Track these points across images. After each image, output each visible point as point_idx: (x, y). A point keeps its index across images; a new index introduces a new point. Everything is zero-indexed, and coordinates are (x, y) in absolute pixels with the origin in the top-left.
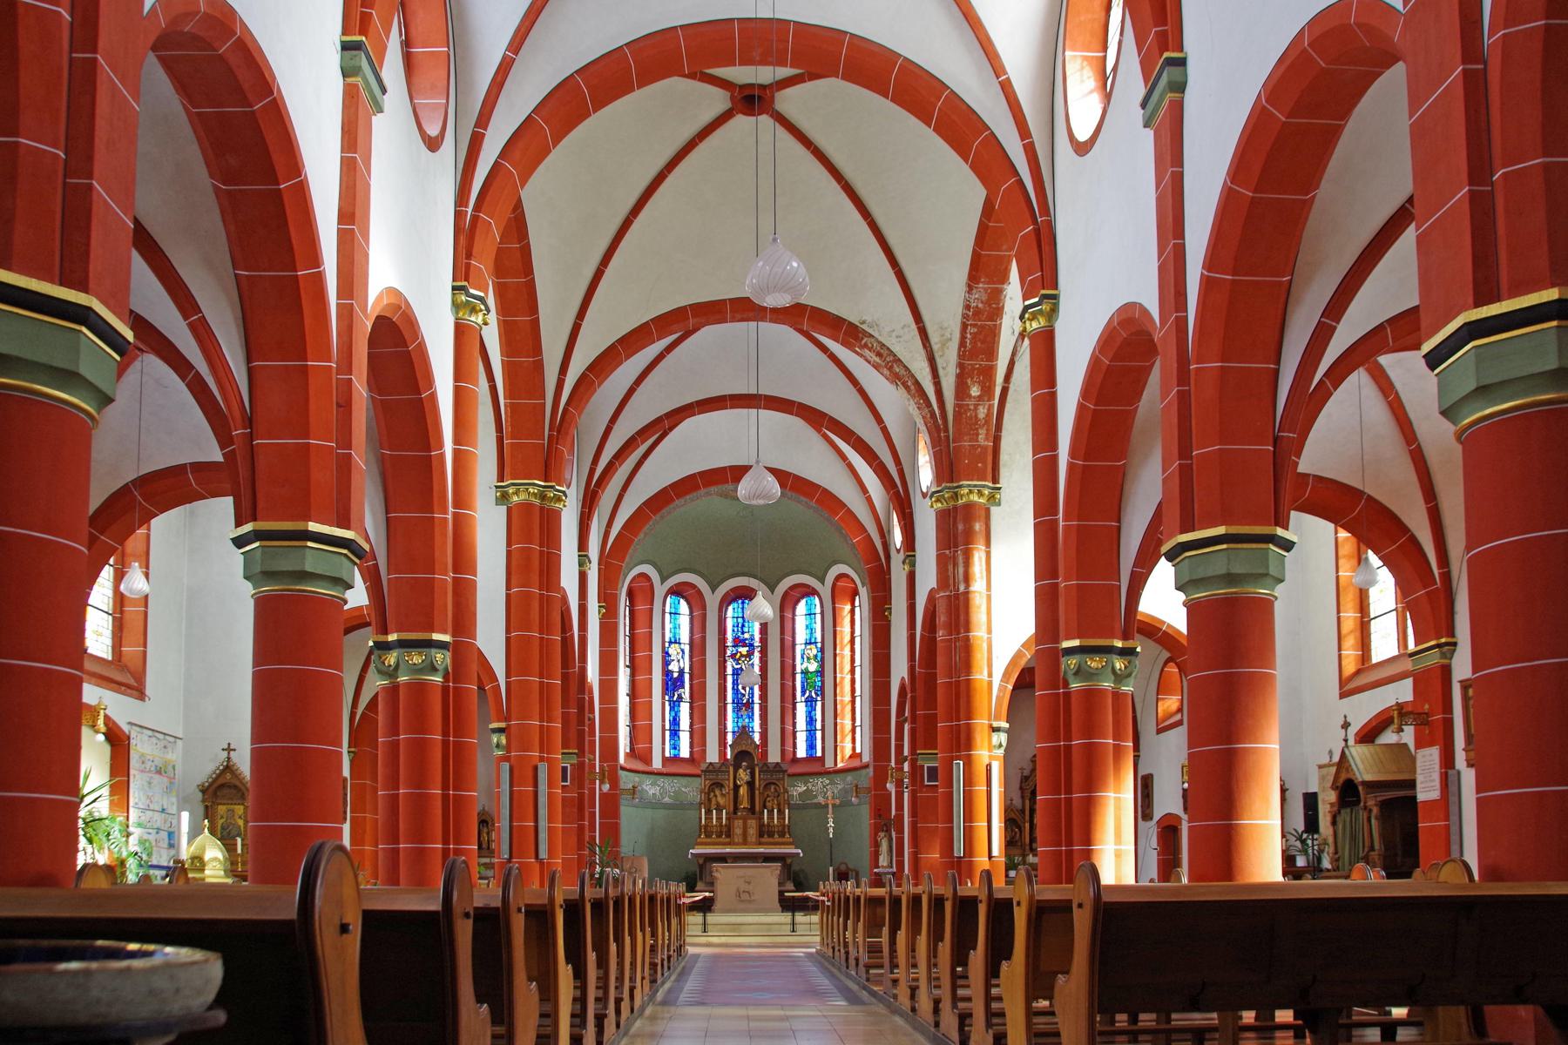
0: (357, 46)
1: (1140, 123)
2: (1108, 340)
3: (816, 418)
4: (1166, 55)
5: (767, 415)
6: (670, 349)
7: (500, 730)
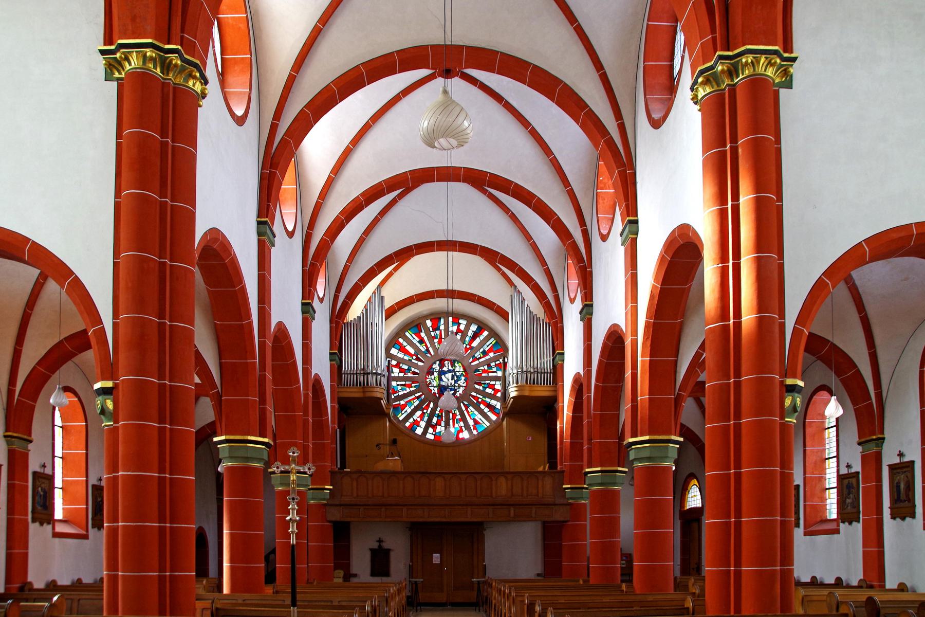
0: (265, 223)
2: (670, 243)
3: (492, 257)
4: (718, 53)
5: (457, 255)
6: (390, 275)
7: (104, 391)
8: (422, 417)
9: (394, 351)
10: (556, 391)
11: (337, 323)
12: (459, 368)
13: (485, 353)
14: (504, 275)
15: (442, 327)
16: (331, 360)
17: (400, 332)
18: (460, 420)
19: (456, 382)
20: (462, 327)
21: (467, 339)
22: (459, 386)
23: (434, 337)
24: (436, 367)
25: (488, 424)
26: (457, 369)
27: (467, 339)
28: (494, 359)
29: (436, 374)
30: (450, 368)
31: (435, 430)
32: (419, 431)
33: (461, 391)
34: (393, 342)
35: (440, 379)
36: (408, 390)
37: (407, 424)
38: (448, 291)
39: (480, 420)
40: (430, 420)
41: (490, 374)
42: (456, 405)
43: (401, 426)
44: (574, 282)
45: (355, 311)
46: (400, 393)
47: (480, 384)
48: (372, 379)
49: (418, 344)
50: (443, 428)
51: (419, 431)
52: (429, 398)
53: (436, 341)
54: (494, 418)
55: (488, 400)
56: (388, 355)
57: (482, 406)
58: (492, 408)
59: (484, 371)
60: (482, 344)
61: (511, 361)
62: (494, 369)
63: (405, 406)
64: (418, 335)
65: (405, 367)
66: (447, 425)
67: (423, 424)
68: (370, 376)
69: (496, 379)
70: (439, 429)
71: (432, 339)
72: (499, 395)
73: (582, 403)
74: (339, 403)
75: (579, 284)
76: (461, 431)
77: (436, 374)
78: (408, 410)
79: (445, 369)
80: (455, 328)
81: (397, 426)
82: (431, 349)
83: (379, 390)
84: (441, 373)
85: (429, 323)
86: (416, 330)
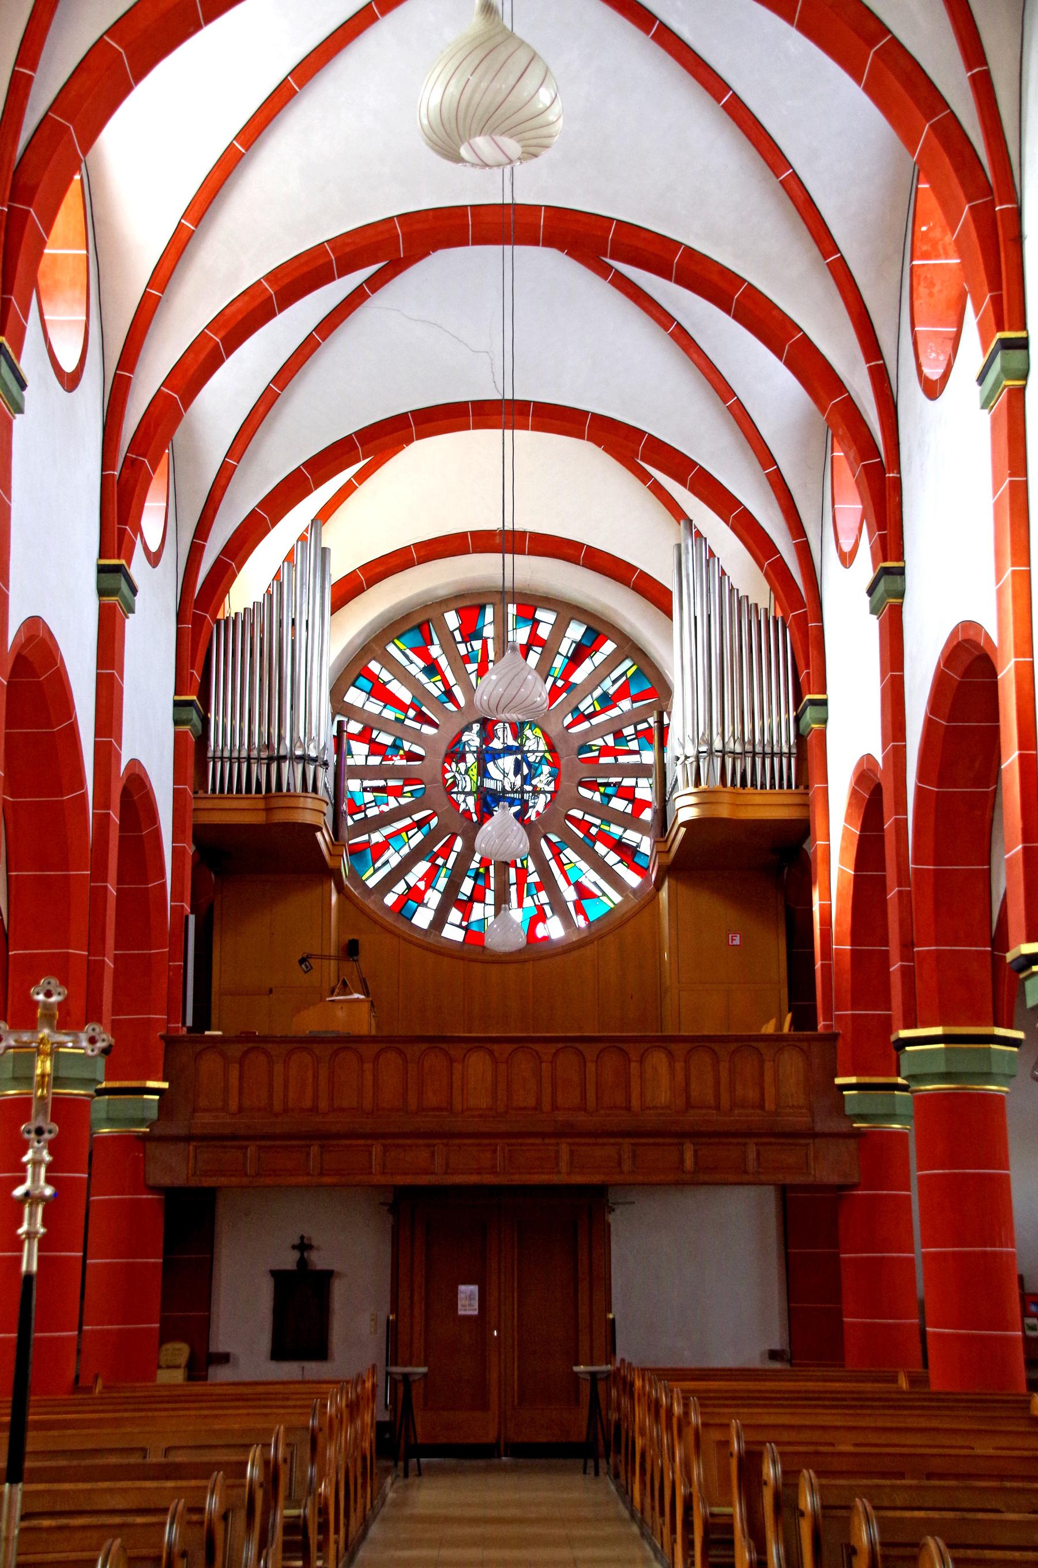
1: (977, 402)
8: (430, 877)
9: (355, 697)
10: (806, 806)
11: (198, 622)
12: (534, 743)
14: (658, 490)
15: (489, 631)
16: (177, 722)
18: (539, 887)
22: (536, 792)
23: (467, 659)
24: (472, 739)
25: (617, 898)
26: (530, 745)
29: (470, 759)
30: (511, 742)
32: (423, 918)
33: (540, 806)
35: (483, 773)
36: (393, 803)
37: (390, 899)
38: (503, 533)
39: (599, 888)
40: (453, 885)
43: (370, 903)
44: (852, 508)
46: (372, 812)
47: (593, 786)
48: (291, 774)
49: (423, 678)
50: (490, 911)
51: (423, 918)
52: (451, 828)
53: (472, 667)
54: (633, 880)
55: (616, 830)
56: (339, 706)
57: (600, 848)
58: (627, 853)
59: (605, 751)
63: (380, 849)
64: (422, 652)
66: (501, 901)
67: (433, 898)
68: (286, 766)
69: (640, 771)
70: (478, 911)
72: (647, 815)
75: (864, 516)
76: (540, 917)
77: (470, 759)
78: (393, 858)
79: (496, 744)
81: (358, 905)
83: (310, 803)
85: (452, 620)
86: (417, 639)
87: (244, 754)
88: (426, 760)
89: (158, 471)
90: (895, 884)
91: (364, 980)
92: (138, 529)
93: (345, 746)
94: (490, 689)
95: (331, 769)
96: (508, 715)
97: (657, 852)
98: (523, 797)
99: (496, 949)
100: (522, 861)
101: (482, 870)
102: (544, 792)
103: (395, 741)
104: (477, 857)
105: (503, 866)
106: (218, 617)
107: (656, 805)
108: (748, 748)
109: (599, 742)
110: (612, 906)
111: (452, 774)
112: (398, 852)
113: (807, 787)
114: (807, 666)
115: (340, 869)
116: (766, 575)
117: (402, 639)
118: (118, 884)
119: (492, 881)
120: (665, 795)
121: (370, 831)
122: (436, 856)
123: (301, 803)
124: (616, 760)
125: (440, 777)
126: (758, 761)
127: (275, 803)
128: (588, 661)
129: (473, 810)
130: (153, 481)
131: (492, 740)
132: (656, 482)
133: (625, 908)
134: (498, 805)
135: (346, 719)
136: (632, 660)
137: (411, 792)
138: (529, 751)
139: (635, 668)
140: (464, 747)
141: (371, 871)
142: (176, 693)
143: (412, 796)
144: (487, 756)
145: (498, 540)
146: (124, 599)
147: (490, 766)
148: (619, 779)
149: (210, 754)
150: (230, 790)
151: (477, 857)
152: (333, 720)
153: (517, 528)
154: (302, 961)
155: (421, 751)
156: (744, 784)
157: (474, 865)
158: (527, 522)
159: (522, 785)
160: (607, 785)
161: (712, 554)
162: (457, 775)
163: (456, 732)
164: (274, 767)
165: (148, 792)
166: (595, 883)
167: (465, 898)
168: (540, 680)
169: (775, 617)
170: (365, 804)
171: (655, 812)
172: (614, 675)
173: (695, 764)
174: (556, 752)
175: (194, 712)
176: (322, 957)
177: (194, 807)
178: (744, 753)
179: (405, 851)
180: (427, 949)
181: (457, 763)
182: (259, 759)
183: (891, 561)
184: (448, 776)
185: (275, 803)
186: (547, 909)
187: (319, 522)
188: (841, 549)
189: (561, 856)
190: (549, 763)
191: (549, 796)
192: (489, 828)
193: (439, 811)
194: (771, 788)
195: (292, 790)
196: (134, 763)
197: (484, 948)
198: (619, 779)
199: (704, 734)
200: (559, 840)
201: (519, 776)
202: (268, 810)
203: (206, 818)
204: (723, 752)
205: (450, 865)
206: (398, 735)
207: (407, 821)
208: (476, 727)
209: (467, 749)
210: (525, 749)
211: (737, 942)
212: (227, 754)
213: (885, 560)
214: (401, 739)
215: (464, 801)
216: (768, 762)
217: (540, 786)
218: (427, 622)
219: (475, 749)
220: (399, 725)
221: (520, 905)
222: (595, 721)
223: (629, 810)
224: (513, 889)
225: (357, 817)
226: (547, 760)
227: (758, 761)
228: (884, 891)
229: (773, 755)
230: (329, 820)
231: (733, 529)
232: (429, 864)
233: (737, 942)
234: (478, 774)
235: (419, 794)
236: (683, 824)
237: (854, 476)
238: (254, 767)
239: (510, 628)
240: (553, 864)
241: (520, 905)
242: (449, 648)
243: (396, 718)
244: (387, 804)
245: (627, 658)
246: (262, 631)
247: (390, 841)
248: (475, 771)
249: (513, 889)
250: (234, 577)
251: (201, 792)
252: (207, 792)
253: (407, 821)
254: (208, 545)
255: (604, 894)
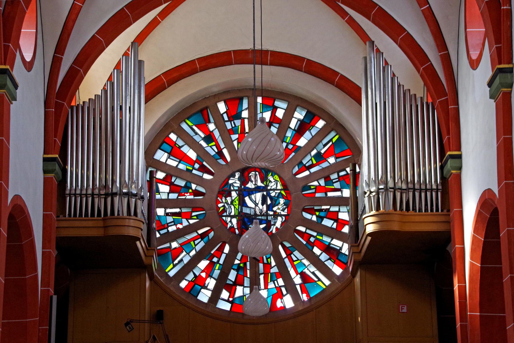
8: (209, 270)
9: (161, 156)
10: (448, 222)
11: (59, 107)
12: (274, 184)
13: (320, 158)
14: (352, 23)
15: (245, 114)
16: (45, 172)
17: (172, 123)
18: (278, 275)
19: (269, 208)
20: (280, 114)
21: (289, 134)
22: (276, 215)
23: (232, 131)
24: (235, 182)
25: (327, 282)
26: (272, 186)
27: (289, 134)
28: (337, 168)
29: (234, 194)
30: (259, 184)
31: (232, 292)
32: (204, 296)
33: (278, 224)
34: (158, 140)
35: (243, 203)
36: (185, 223)
37: (184, 284)
38: (254, 51)
39: (314, 275)
40: (224, 275)
41: (330, 194)
42: (269, 247)
43: (171, 287)
44: (478, 31)
45: (92, 84)
46: (172, 229)
47: (311, 211)
48: (120, 204)
49: (203, 144)
50: (247, 291)
51: (204, 296)
52: (220, 237)
53: (235, 137)
54: (337, 270)
55: (326, 239)
56: (151, 162)
57: (317, 251)
58: (334, 254)
59: (318, 189)
60: (313, 143)
61: (366, 171)
62: (337, 185)
63: (177, 252)
64: (203, 127)
65: (181, 183)
66: (254, 284)
67: (211, 283)
68: (117, 199)
69: (341, 201)
70: (239, 291)
71: (226, 134)
72: (346, 229)
73: (499, 244)
74: (58, 247)
75: (486, 35)
76: (279, 295)
77: (234, 194)
78: (185, 258)
79: (250, 185)
80: (267, 116)
81: (164, 287)
82: (225, 152)
83: (132, 223)
84: (244, 192)
85: (222, 107)
86: (200, 119)
87: (90, 192)
88: (206, 196)
89: (30, 8)
90: (509, 271)
91: (167, 336)
92: (18, 46)
93: (154, 188)
94: (247, 147)
95: (146, 201)
96: (259, 163)
97: (353, 253)
98: (267, 218)
99: (250, 314)
100: (267, 259)
101: (242, 265)
102: (281, 216)
103: (186, 184)
104: (239, 256)
105: (255, 261)
106: (72, 104)
107: (352, 223)
108: (411, 186)
109: (316, 183)
110: (324, 287)
111: (222, 204)
112: (188, 254)
113: (449, 211)
114: (448, 134)
115: (152, 265)
116: (422, 76)
117: (190, 120)
118: (5, 276)
119: (248, 271)
120: (358, 216)
121: (171, 241)
122: (213, 256)
123: (127, 222)
124: (326, 194)
125: (215, 207)
126: (417, 194)
127: (109, 223)
128: (307, 132)
129: (235, 227)
130: (27, 15)
131: (248, 183)
132: (351, 17)
133: (333, 289)
134: (252, 224)
135: (155, 170)
136: (336, 131)
137: (196, 216)
138: (271, 190)
139: (337, 137)
140: (230, 187)
141: (171, 266)
142: (45, 153)
143: (197, 219)
144: (244, 193)
145: (250, 56)
146: (9, 90)
147: (247, 199)
148: (328, 207)
149: (68, 192)
150: (81, 215)
151: (239, 256)
152: (147, 171)
153: (264, 48)
154: (127, 324)
155: (203, 190)
156: (408, 209)
157: (237, 262)
158: (270, 44)
159: (267, 211)
160: (320, 210)
161: (386, 63)
162: (226, 204)
163: (225, 177)
164: (109, 199)
165: (26, 216)
166: (313, 273)
167: (231, 283)
168: (279, 141)
169: (427, 103)
170: (167, 224)
171: (351, 228)
172: (325, 141)
173: (376, 196)
174: (288, 190)
175: (57, 165)
176: (139, 321)
177: (56, 226)
178: (408, 189)
179: (193, 253)
180: (207, 316)
181: (226, 198)
182: (99, 195)
183: (504, 64)
184: (220, 205)
185: (109, 223)
186: (283, 290)
187: (137, 44)
188: (471, 58)
189: (292, 255)
190: (283, 197)
191: (284, 217)
192: (247, 236)
193: (215, 228)
194: (425, 211)
195: (121, 215)
196: (17, 197)
197: (243, 314)
198: (328, 207)
199: (382, 177)
200: (290, 245)
201: (265, 206)
202: (105, 227)
203: (65, 233)
204: (394, 189)
205: (221, 262)
206: (188, 180)
207: (195, 235)
208: (237, 175)
209: (232, 188)
210: (269, 188)
211: (405, 310)
212: (78, 192)
213: (500, 63)
214: (191, 183)
215: (231, 221)
216: (423, 195)
217: (278, 211)
218: (206, 108)
219: (237, 188)
220: (189, 174)
221: (266, 287)
222: (313, 170)
223: (335, 226)
224: (262, 277)
225: (163, 232)
226: (283, 195)
227: (417, 194)
228: (501, 277)
229: (426, 190)
230: (145, 233)
231: (400, 46)
232: (208, 262)
233: (405, 310)
234: (239, 204)
235: (201, 218)
236: (370, 234)
237: (480, 9)
238: (96, 200)
239: (259, 112)
240: (287, 261)
241: (266, 287)
242: (221, 125)
243: (187, 169)
244: (181, 224)
245: (332, 130)
246: (101, 114)
247: (183, 247)
248: (237, 202)
249: (262, 277)
250: (82, 78)
251: (61, 216)
252: (65, 216)
253: (195, 235)
254: (64, 57)
255: (319, 280)
